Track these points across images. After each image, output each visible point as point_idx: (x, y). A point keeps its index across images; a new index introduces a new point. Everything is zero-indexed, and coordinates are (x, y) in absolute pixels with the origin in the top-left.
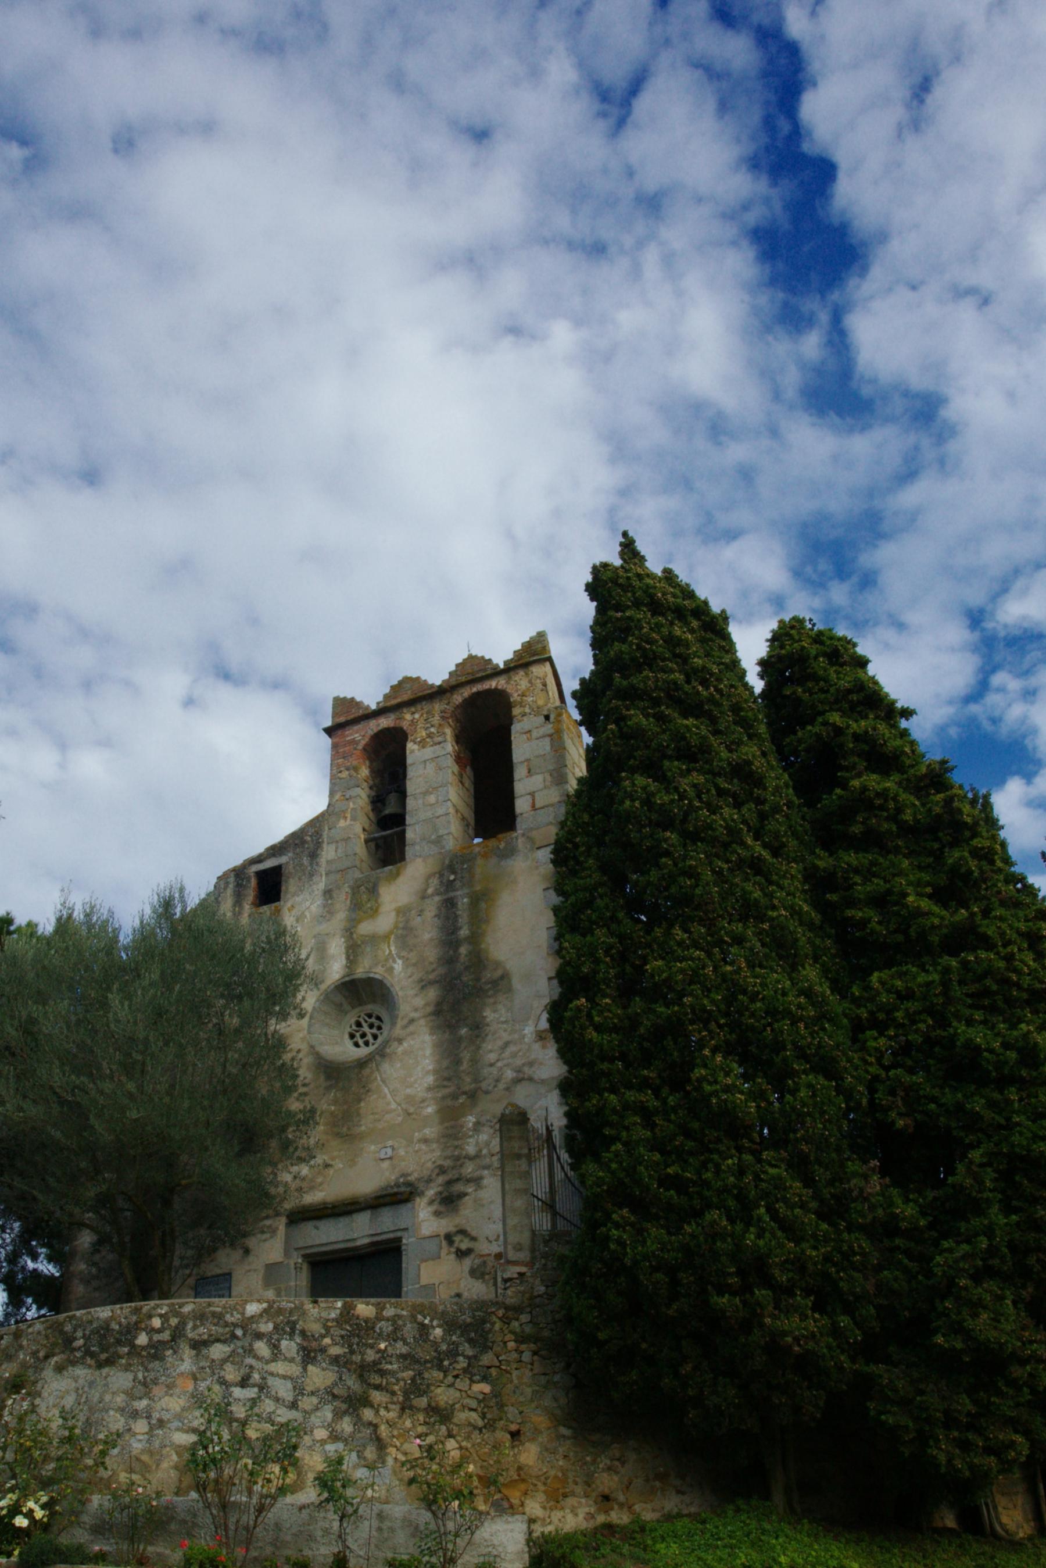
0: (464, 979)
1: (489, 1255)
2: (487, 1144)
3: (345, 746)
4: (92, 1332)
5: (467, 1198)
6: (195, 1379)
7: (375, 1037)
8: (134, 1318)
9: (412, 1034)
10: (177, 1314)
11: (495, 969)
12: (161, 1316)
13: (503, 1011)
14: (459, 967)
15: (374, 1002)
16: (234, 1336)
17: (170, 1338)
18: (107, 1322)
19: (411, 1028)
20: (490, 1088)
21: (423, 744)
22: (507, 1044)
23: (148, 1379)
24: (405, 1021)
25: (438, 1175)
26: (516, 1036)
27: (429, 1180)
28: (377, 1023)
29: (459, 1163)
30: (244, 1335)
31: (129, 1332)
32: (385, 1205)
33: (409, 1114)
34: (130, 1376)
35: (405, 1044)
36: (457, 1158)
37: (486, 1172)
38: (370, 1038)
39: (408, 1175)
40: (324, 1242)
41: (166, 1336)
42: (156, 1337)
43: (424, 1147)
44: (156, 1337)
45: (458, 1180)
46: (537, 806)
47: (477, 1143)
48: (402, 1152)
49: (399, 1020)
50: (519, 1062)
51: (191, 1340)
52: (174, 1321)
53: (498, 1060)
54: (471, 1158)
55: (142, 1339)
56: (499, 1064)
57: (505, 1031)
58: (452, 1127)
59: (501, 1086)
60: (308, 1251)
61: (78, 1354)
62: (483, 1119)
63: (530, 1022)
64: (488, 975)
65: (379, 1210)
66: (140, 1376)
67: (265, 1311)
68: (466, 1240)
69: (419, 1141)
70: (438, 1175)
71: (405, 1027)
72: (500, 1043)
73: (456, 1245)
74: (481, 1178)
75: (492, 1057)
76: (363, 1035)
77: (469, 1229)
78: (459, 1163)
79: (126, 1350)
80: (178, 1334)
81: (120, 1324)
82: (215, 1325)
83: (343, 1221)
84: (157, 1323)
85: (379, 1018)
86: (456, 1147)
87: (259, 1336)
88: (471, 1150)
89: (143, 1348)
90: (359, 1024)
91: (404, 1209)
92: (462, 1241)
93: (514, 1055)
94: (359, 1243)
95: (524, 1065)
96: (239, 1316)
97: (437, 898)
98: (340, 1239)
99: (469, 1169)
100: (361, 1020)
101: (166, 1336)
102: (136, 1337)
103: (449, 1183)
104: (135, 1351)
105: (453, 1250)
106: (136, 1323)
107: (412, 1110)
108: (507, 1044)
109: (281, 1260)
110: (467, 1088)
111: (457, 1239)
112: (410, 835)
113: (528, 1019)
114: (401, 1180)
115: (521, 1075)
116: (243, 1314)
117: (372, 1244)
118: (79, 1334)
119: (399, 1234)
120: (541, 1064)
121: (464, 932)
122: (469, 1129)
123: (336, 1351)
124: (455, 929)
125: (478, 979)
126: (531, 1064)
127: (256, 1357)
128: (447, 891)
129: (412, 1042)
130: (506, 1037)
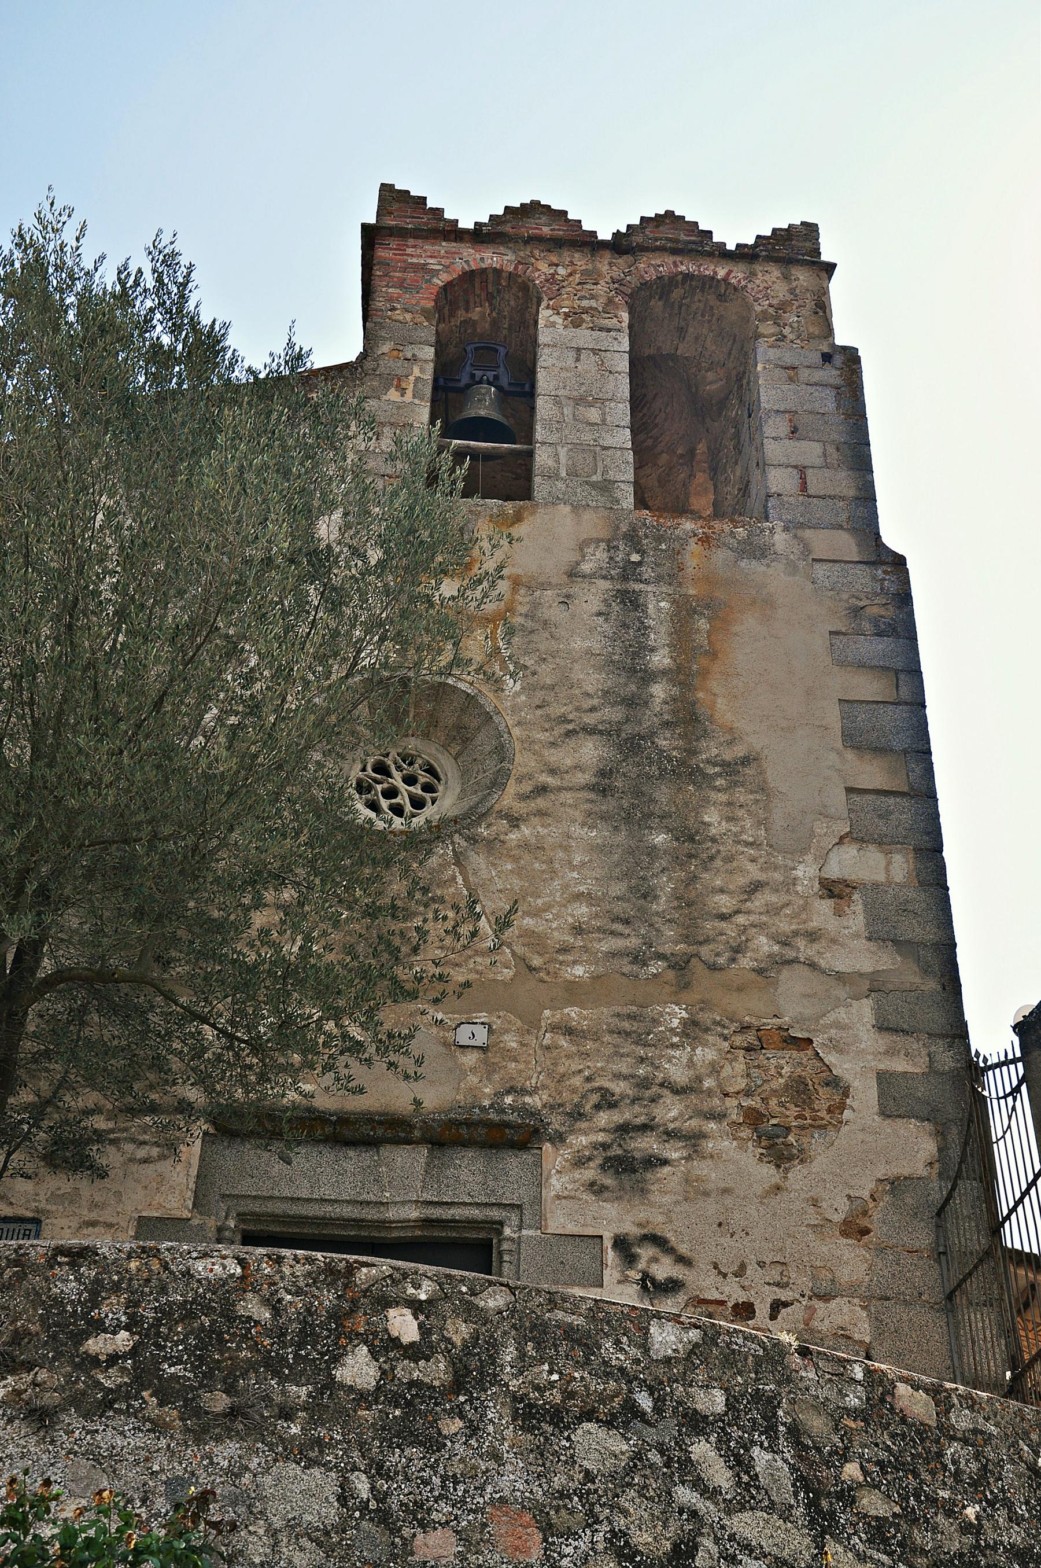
0: (662, 743)
1: (722, 1303)
2: (715, 1069)
3: (404, 270)
4: (165, 1312)
5: (667, 1169)
6: (548, 1529)
7: (418, 804)
8: (328, 1298)
9: (541, 813)
10: (469, 1311)
11: (730, 743)
12: (416, 1307)
13: (748, 823)
14: (649, 720)
15: (426, 736)
16: (631, 1409)
17: (448, 1378)
18: (227, 1292)
19: (541, 803)
20: (721, 961)
21: (574, 319)
22: (756, 887)
23: (394, 1503)
24: (527, 787)
25: (598, 1107)
26: (778, 876)
27: (577, 1115)
28: (424, 778)
29: (648, 1093)
30: (658, 1409)
31: (307, 1335)
32: (466, 1144)
33: (531, 969)
34: (323, 1482)
35: (526, 830)
36: (644, 1083)
37: (712, 1125)
38: (403, 800)
39: (524, 1092)
40: (304, 1194)
41: (436, 1371)
42: (407, 1371)
43: (563, 1042)
44: (407, 1371)
45: (645, 1128)
46: (811, 491)
47: (691, 1064)
48: (511, 1042)
49: (512, 781)
50: (785, 926)
51: (515, 1399)
52: (459, 1331)
53: (738, 912)
54: (678, 1091)
55: (359, 1369)
56: (741, 919)
57: (753, 860)
58: (631, 1017)
59: (746, 962)
60: (256, 1207)
61: (111, 1379)
62: (706, 1018)
63: (809, 858)
64: (711, 749)
65: (449, 1152)
66: (362, 1485)
67: (694, 1349)
68: (667, 1260)
69: (554, 1028)
70: (598, 1107)
71: (524, 797)
72: (742, 881)
73: (642, 1265)
74: (702, 1135)
75: (725, 902)
76: (391, 793)
77: (669, 1235)
78: (648, 1093)
79: (301, 1392)
80: (471, 1374)
81: (276, 1307)
82: (578, 1365)
83: (354, 1160)
84: (404, 1325)
85: (431, 771)
86: (642, 1060)
87: (696, 1423)
88: (679, 1075)
89: (363, 1398)
90: (381, 769)
91: (513, 1163)
92: (655, 1260)
93: (775, 911)
94: (391, 1214)
95: (796, 933)
96: (634, 1352)
97: (604, 585)
98: (345, 1197)
99: (670, 1111)
100: (389, 762)
101: (436, 1371)
102: (336, 1359)
103: (624, 1129)
104: (330, 1400)
105: (635, 1275)
106: (335, 1315)
107: (537, 961)
108: (756, 887)
109: (186, 1214)
110: (667, 949)
111: (645, 1253)
112: (542, 458)
113: (804, 851)
114: (509, 1100)
115: (791, 954)
116: (646, 1348)
117: (427, 1222)
118: (113, 1309)
119: (495, 1214)
120: (834, 941)
121: (661, 659)
122: (672, 1030)
123: (874, 1504)
124: (641, 649)
125: (693, 752)
126: (813, 936)
127: (699, 1485)
128: (624, 578)
129: (543, 831)
130: (754, 872)
